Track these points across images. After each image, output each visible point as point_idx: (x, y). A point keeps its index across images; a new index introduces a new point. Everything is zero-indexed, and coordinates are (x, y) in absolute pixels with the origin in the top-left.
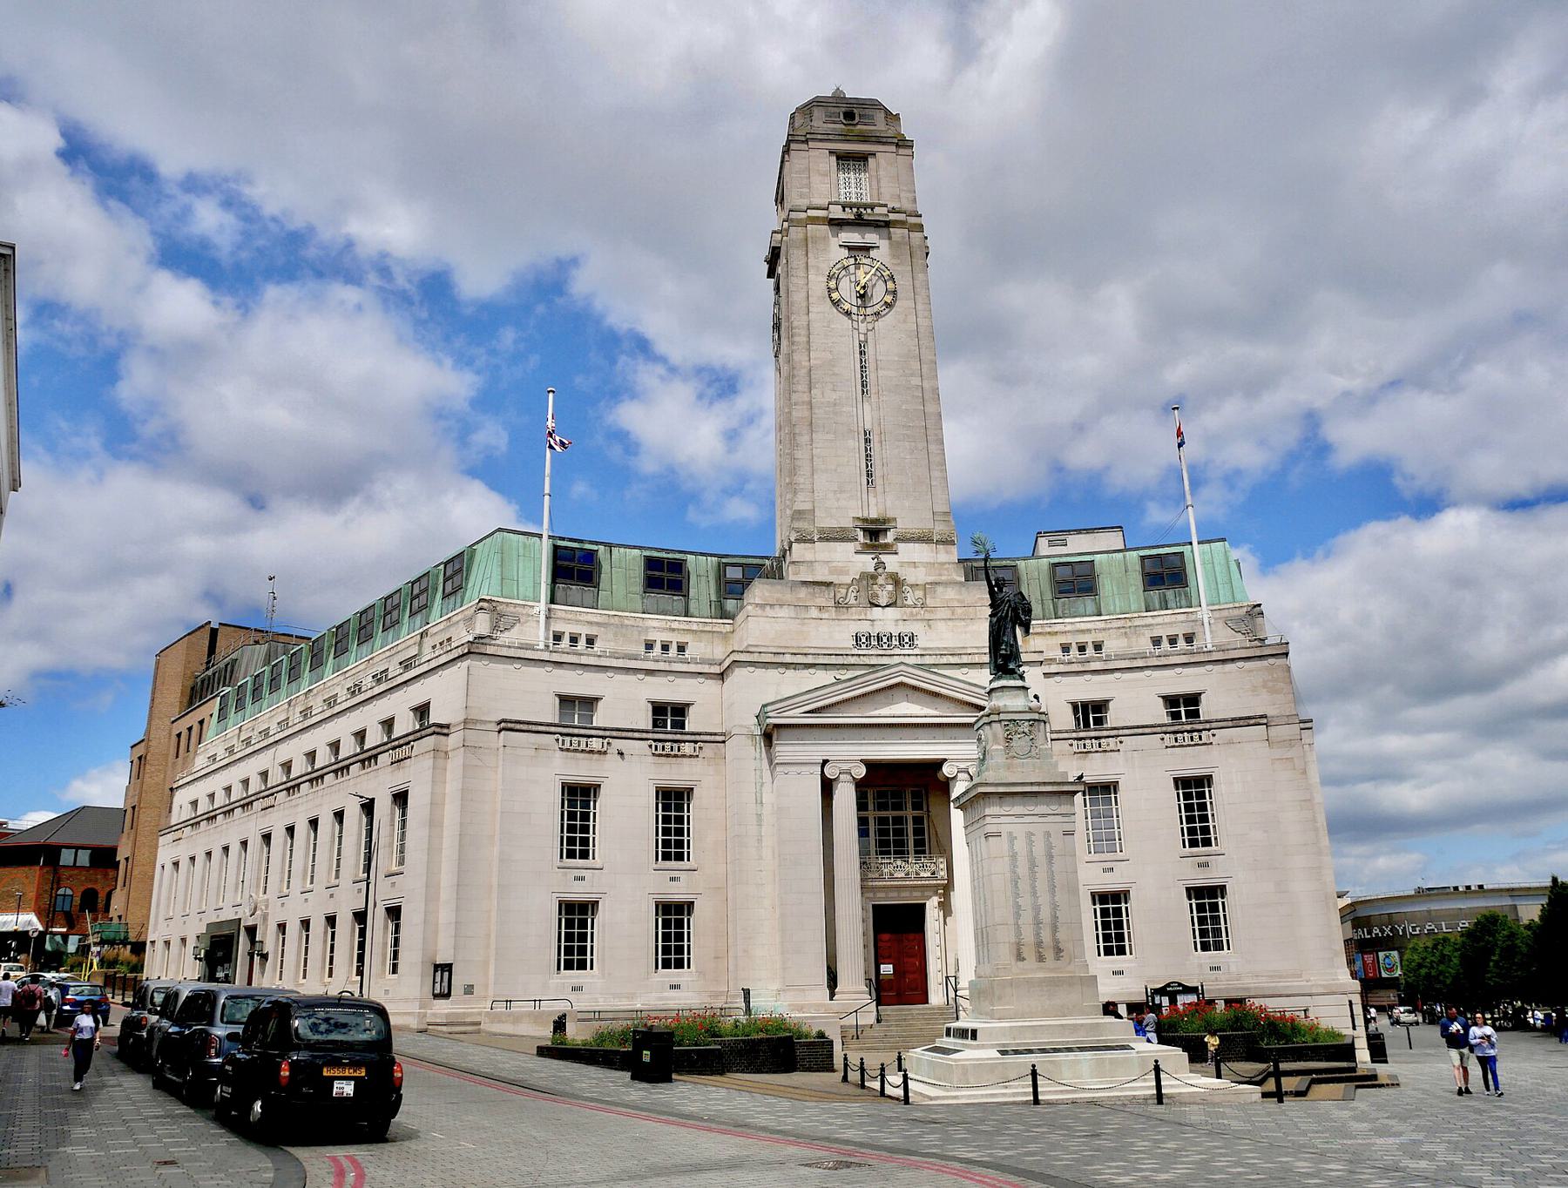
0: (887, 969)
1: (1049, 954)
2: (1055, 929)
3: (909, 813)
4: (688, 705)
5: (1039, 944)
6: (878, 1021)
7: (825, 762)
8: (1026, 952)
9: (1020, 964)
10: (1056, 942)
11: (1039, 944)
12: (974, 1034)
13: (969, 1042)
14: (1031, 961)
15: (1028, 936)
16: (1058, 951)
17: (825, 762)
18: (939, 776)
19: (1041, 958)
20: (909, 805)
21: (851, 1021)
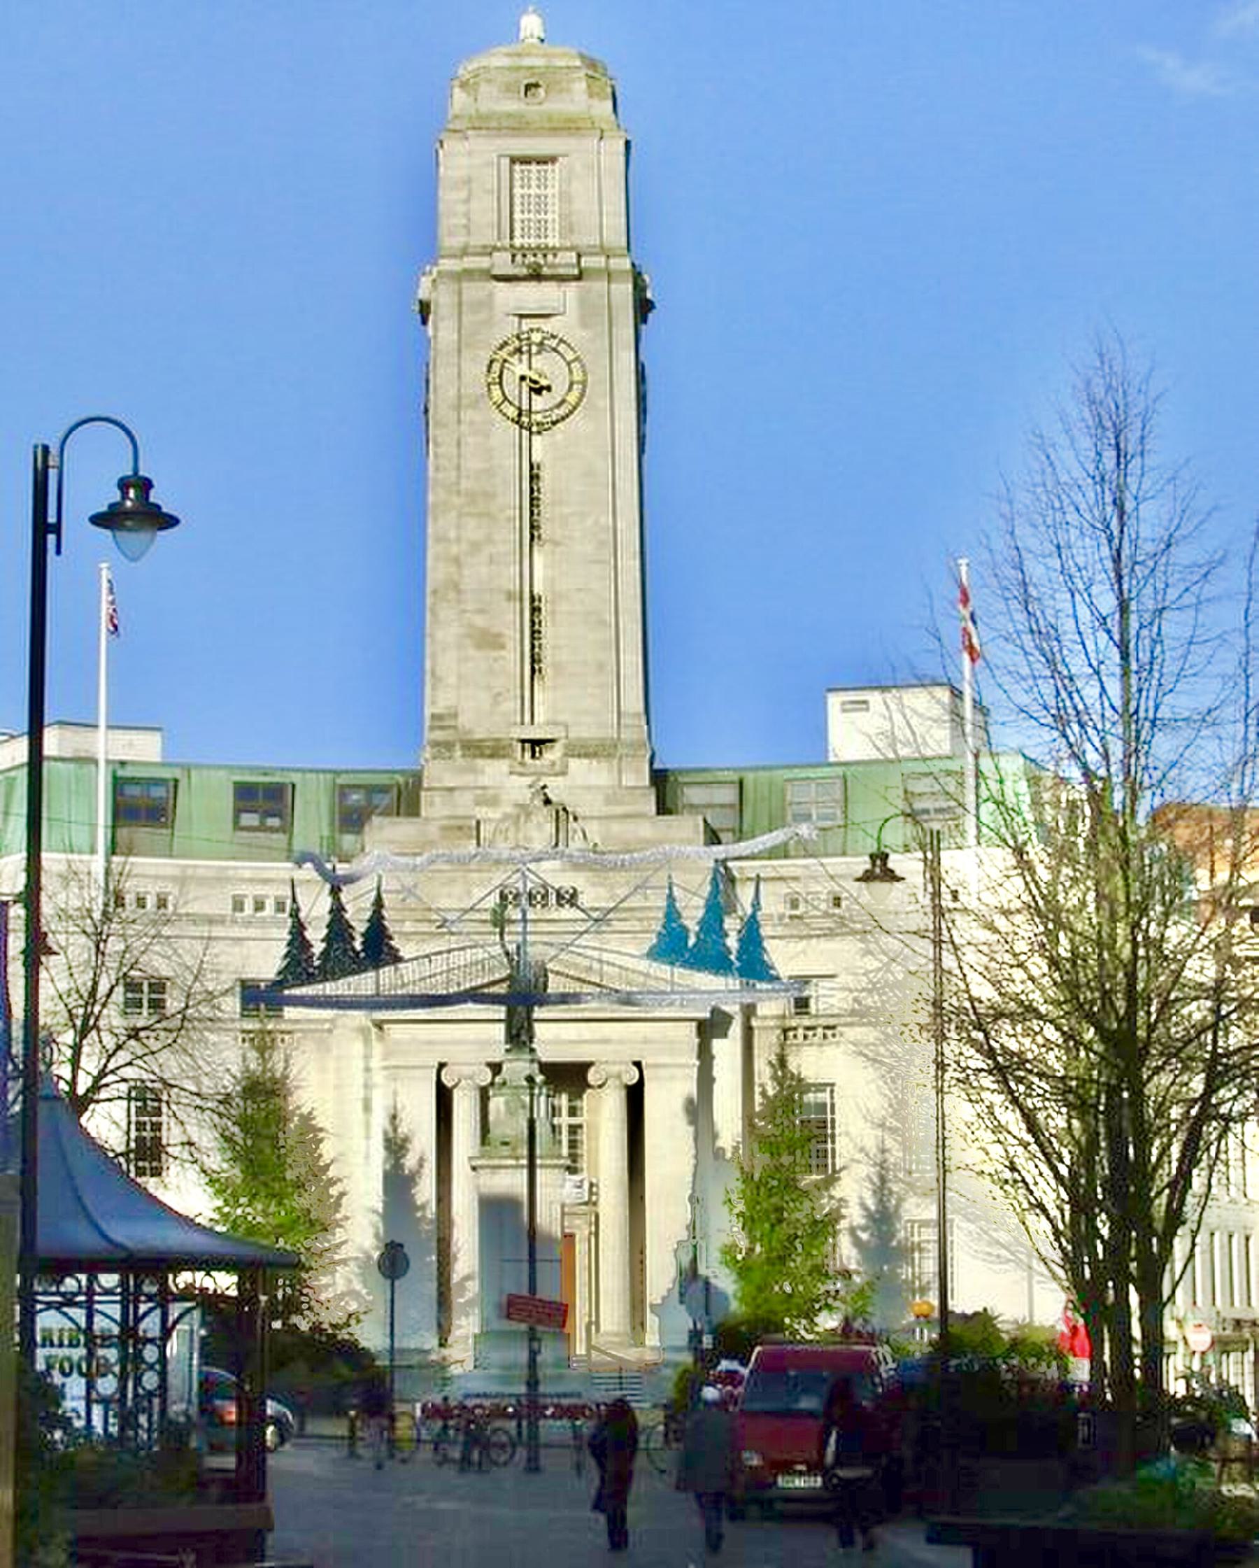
4: (590, 1064)
7: (442, 1066)
17: (442, 1066)
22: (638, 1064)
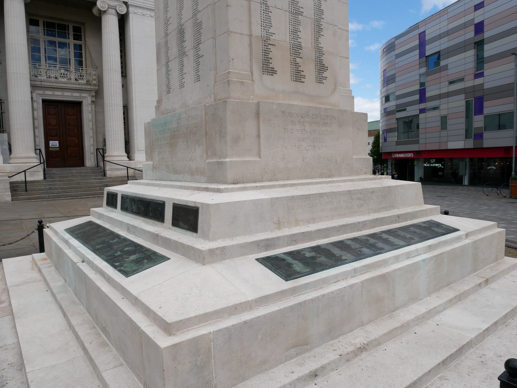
0: (54, 144)
1: (309, 70)
2: (318, 30)
3: (71, 41)
5: (296, 49)
6: (45, 178)
8: (280, 59)
9: (267, 78)
10: (319, 51)
11: (296, 49)
12: (187, 217)
13: (166, 230)
14: (282, 81)
15: (281, 32)
16: (321, 67)
18: (95, 11)
19: (298, 76)
20: (71, 37)
21: (20, 178)
22: (126, 3)
